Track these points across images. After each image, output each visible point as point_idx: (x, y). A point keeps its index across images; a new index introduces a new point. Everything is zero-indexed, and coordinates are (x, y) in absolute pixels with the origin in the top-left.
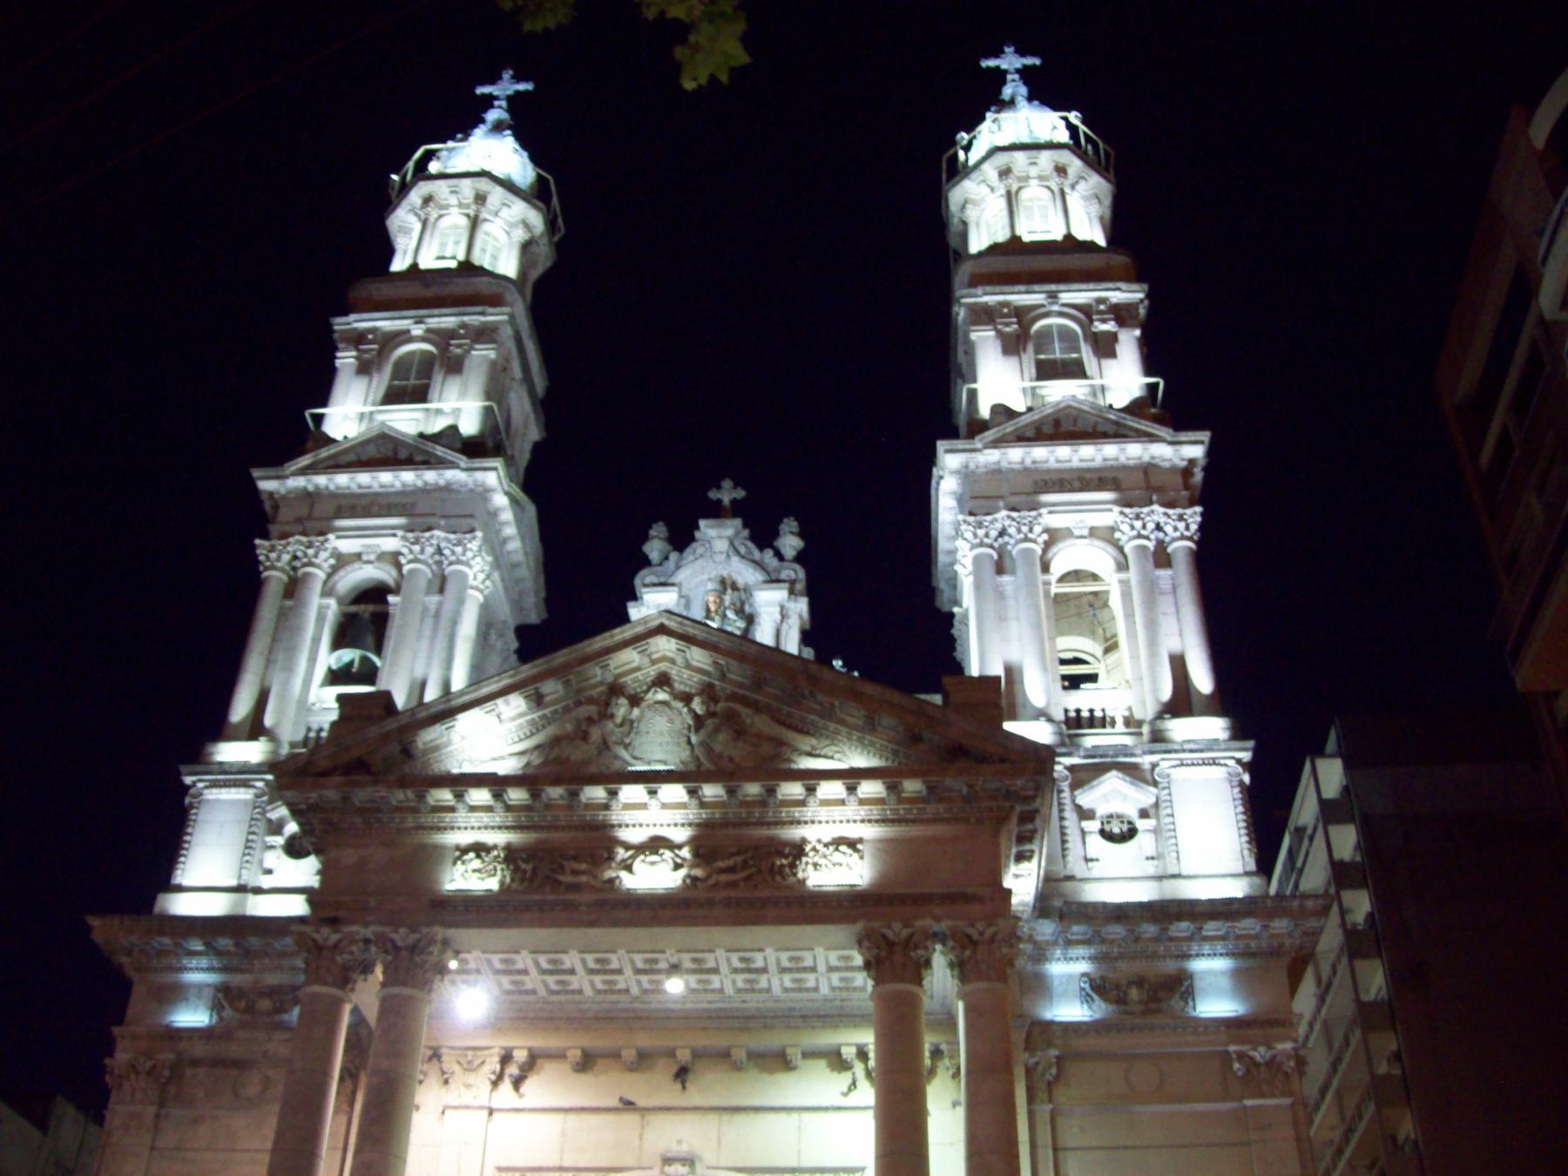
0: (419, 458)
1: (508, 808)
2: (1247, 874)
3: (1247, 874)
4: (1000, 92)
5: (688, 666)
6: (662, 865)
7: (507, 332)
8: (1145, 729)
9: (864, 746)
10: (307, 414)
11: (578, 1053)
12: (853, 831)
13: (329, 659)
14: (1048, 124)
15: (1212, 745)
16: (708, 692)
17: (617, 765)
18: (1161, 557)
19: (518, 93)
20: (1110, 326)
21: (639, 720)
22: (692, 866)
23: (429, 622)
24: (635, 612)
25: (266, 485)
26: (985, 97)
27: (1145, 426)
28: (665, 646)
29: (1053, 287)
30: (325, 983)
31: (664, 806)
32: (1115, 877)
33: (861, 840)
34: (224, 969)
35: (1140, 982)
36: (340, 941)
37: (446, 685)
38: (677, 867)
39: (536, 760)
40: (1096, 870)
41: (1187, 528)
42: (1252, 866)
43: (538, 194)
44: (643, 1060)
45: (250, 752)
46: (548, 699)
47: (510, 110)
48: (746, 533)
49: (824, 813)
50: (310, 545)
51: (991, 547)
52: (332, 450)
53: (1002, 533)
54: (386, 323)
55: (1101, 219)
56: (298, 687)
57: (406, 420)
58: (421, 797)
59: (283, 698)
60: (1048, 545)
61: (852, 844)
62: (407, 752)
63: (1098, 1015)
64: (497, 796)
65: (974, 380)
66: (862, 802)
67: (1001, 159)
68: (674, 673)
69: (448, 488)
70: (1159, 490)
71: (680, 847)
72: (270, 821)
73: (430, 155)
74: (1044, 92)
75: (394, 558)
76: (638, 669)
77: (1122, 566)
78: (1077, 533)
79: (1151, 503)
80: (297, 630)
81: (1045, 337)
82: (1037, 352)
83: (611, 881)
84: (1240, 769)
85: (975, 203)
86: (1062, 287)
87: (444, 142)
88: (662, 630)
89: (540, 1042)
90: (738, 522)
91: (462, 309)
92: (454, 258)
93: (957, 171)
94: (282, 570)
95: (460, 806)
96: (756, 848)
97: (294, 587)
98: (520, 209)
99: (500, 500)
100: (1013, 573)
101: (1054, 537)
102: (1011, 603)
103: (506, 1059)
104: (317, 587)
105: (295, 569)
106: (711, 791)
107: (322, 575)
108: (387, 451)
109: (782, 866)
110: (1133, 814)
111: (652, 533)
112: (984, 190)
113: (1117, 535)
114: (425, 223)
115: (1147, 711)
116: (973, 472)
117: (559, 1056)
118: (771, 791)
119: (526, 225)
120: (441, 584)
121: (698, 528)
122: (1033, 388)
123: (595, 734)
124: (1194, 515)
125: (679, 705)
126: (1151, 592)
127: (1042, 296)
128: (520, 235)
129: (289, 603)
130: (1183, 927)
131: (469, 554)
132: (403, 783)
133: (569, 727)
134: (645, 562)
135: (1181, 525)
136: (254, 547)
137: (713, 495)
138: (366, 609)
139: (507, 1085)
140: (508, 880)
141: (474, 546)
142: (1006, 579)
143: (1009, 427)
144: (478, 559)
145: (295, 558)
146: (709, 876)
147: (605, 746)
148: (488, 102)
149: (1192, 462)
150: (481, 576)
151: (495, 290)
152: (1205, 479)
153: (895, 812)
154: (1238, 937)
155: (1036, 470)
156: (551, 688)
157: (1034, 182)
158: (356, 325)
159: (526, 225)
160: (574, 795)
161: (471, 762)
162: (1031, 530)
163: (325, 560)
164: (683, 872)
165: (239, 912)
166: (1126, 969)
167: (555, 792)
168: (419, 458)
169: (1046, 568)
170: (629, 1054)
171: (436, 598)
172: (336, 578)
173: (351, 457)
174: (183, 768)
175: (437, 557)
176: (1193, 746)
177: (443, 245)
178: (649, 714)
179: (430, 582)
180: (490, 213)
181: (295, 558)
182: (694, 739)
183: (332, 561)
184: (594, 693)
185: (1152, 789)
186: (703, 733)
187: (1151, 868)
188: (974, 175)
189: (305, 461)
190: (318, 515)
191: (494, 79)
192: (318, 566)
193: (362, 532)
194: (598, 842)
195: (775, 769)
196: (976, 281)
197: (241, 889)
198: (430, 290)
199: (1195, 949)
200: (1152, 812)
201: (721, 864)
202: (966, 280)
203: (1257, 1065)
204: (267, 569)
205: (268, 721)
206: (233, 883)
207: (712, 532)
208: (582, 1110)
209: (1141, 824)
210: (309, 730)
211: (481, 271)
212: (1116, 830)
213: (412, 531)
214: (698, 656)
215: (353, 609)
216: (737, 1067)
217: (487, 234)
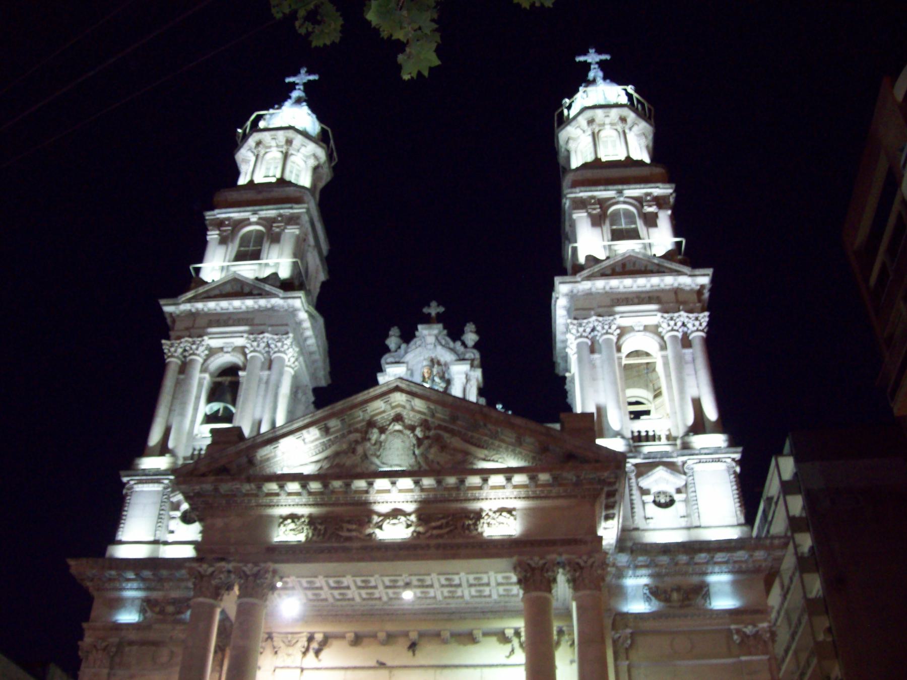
0: (255, 292)
2: (739, 525)
3: (739, 525)
4: (587, 75)
5: (413, 409)
6: (400, 525)
7: (305, 218)
8: (679, 442)
9: (515, 454)
10: (191, 267)
11: (352, 635)
12: (510, 504)
13: (205, 409)
14: (616, 93)
15: (717, 450)
16: (425, 425)
17: (373, 468)
18: (686, 342)
19: (309, 81)
20: (653, 209)
21: (385, 441)
23: (263, 386)
25: (168, 309)
26: (579, 78)
27: (675, 266)
29: (620, 187)
30: (205, 596)
32: (662, 528)
33: (514, 509)
34: (147, 589)
35: (678, 589)
36: (213, 572)
37: (273, 423)
38: (408, 526)
39: (326, 465)
40: (651, 524)
41: (701, 324)
42: (742, 520)
43: (322, 139)
44: (390, 639)
45: (161, 463)
46: (332, 430)
47: (305, 91)
48: (445, 332)
49: (493, 494)
50: (194, 343)
51: (587, 337)
52: (206, 288)
53: (593, 330)
54: (235, 214)
55: (647, 147)
56: (188, 425)
57: (248, 270)
58: (260, 488)
60: (620, 336)
61: (510, 511)
62: (251, 462)
64: (304, 486)
65: (576, 242)
66: (515, 487)
67: (589, 114)
68: (405, 413)
69: (273, 309)
70: (684, 303)
71: (410, 514)
72: (172, 503)
73: (260, 118)
74: (613, 74)
75: (242, 350)
76: (384, 412)
77: (663, 347)
78: (636, 328)
79: (679, 311)
80: (186, 392)
81: (616, 216)
82: (612, 225)
83: (370, 535)
84: (734, 464)
85: (574, 139)
86: (625, 187)
87: (268, 109)
88: (397, 389)
89: (330, 629)
90: (440, 326)
91: (279, 206)
92: (274, 176)
93: (563, 122)
94: (177, 357)
95: (282, 493)
96: (454, 515)
97: (185, 367)
98: (312, 148)
99: (303, 315)
100: (600, 352)
102: (599, 370)
103: (311, 639)
104: (198, 367)
105: (185, 357)
106: (427, 482)
107: (200, 360)
109: (469, 525)
110: (671, 490)
111: (391, 333)
112: (579, 131)
113: (660, 330)
114: (257, 157)
115: (679, 432)
116: (576, 295)
117: (341, 637)
118: (462, 481)
120: (269, 364)
121: (417, 329)
122: (610, 246)
123: (360, 450)
124: (704, 317)
125: (408, 432)
126: (680, 362)
127: (614, 192)
128: (312, 163)
129: (182, 377)
130: (702, 557)
131: (286, 347)
132: (249, 480)
133: (345, 446)
134: (387, 350)
135: (697, 323)
136: (161, 345)
137: (426, 310)
138: (227, 379)
139: (311, 654)
140: (310, 535)
141: (288, 342)
142: (596, 356)
143: (597, 268)
144: (291, 350)
145: (185, 350)
146: (426, 532)
147: (365, 457)
148: (293, 86)
149: (702, 287)
150: (293, 360)
151: (298, 194)
152: (710, 296)
153: (535, 492)
154: (735, 562)
155: (612, 293)
156: (334, 423)
157: (607, 127)
159: (315, 157)
160: (348, 485)
161: (288, 467)
162: (610, 328)
163: (202, 351)
164: (412, 529)
165: (154, 555)
166: (669, 581)
167: (337, 484)
168: (255, 292)
169: (619, 349)
170: (382, 635)
171: (266, 373)
172: (209, 362)
173: (217, 292)
174: (122, 473)
175: (267, 349)
176: (706, 451)
177: (268, 169)
178: (390, 438)
179: (263, 363)
181: (185, 350)
182: (417, 452)
183: (207, 352)
184: (359, 426)
185: (684, 477)
186: (422, 448)
187: (683, 522)
188: (574, 123)
189: (190, 295)
190: (198, 326)
192: (199, 355)
193: (223, 335)
194: (362, 513)
195: (464, 469)
196: (576, 184)
197: (156, 542)
198: (260, 195)
199: (710, 569)
200: (683, 490)
201: (433, 524)
202: (569, 184)
203: (748, 637)
204: (169, 357)
205: (171, 445)
206: (151, 539)
207: (425, 332)
208: (355, 668)
209: (677, 497)
210: (194, 449)
211: (290, 184)
212: (663, 501)
213: (252, 334)
214: (419, 404)
215: (219, 379)
216: (445, 642)
217: (294, 163)
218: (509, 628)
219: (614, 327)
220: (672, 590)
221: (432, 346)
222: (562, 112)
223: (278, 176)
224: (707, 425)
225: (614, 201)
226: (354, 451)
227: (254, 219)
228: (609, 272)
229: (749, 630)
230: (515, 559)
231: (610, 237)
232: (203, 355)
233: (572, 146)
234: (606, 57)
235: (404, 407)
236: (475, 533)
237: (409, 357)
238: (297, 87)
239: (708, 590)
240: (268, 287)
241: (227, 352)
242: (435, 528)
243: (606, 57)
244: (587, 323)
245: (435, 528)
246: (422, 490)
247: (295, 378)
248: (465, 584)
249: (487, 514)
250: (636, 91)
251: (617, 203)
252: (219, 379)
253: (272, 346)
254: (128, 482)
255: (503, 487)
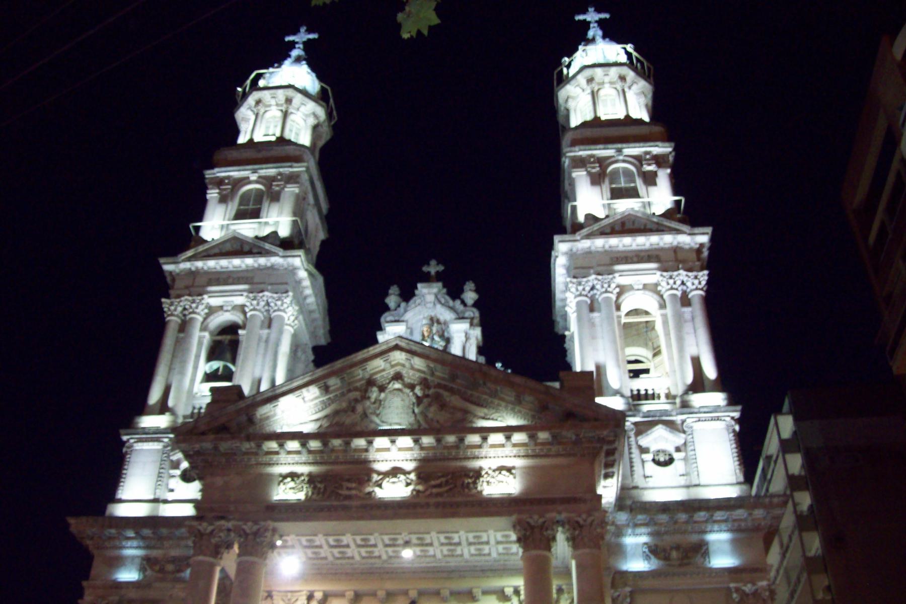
0: (255, 250)
1: (310, 452)
2: (738, 483)
4: (586, 34)
5: (412, 368)
6: (399, 484)
7: (305, 177)
8: (678, 401)
10: (191, 226)
11: (352, 593)
12: (509, 463)
13: (205, 367)
14: (615, 52)
15: (716, 409)
16: (424, 383)
17: (372, 426)
18: (685, 300)
19: (309, 40)
20: (652, 168)
21: (385, 399)
22: (417, 484)
23: (263, 345)
24: (381, 337)
25: (168, 268)
26: (578, 37)
27: (674, 225)
28: (399, 357)
29: (619, 146)
30: (205, 555)
31: (400, 449)
32: (662, 486)
33: (514, 468)
35: (677, 548)
36: (213, 531)
37: (273, 381)
38: (408, 484)
39: (326, 424)
40: (651, 483)
41: (700, 283)
42: (741, 479)
43: (322, 98)
45: (161, 421)
46: (331, 389)
47: (305, 50)
48: (445, 290)
49: (492, 452)
50: (194, 302)
51: (586, 296)
52: (206, 246)
53: (593, 288)
54: (235, 173)
55: (647, 106)
56: (188, 383)
57: (248, 229)
58: (259, 446)
59: (179, 389)
60: (619, 295)
61: (509, 470)
62: (251, 421)
63: (653, 567)
64: (303, 445)
65: (575, 200)
66: (515, 445)
67: (588, 73)
68: (404, 372)
69: (272, 268)
70: (683, 261)
71: (409, 473)
72: (172, 461)
73: (259, 76)
74: (612, 33)
75: (242, 308)
76: (383, 370)
77: (663, 306)
79: (678, 269)
81: (616, 172)
82: (611, 183)
83: (370, 493)
84: (733, 423)
85: (573, 98)
86: (624, 145)
87: (267, 68)
88: (397, 347)
90: (440, 284)
92: (274, 135)
93: (562, 80)
94: (177, 316)
97: (184, 326)
99: (303, 274)
100: (599, 311)
101: (623, 290)
102: (599, 329)
105: (185, 315)
106: (427, 440)
107: (200, 319)
108: (237, 247)
109: (468, 483)
110: (671, 449)
111: (390, 291)
113: (659, 288)
114: (257, 115)
115: (679, 390)
116: (575, 254)
118: (462, 440)
119: (315, 116)
120: (269, 323)
121: (416, 288)
122: (609, 204)
123: (359, 408)
124: (704, 276)
125: (407, 391)
126: (680, 321)
128: (312, 121)
129: (182, 335)
130: (701, 515)
131: (285, 306)
132: (248, 438)
133: (344, 405)
134: (387, 308)
135: (696, 282)
136: (161, 303)
137: (425, 269)
138: (227, 338)
140: (310, 494)
141: (288, 301)
143: (596, 227)
144: (290, 308)
145: (185, 309)
146: (426, 490)
147: (365, 415)
148: (292, 45)
149: (702, 245)
150: (292, 318)
151: (298, 153)
153: (534, 451)
154: (735, 520)
156: (333, 382)
157: (607, 86)
158: (218, 175)
159: (315, 116)
160: (348, 444)
161: (288, 425)
162: (609, 286)
163: (202, 310)
164: (411, 487)
166: (669, 540)
167: (337, 443)
168: (255, 250)
169: (618, 308)
171: (266, 331)
172: (209, 320)
173: (216, 251)
174: (122, 431)
175: (267, 308)
177: (268, 128)
178: (390, 396)
179: (263, 322)
180: (294, 108)
181: (185, 309)
182: (416, 410)
183: (206, 311)
184: (358, 384)
185: (683, 435)
186: (422, 406)
187: (682, 481)
188: (573, 82)
189: (190, 253)
190: (198, 284)
191: (295, 32)
192: (198, 314)
193: (223, 294)
194: (362, 471)
195: (463, 427)
196: (575, 143)
197: (156, 501)
198: (260, 153)
200: (683, 448)
201: (433, 483)
202: (569, 142)
203: (747, 595)
204: (169, 315)
205: (171, 403)
206: (151, 497)
207: (425, 291)
209: (676, 456)
210: (194, 408)
211: (289, 142)
212: (662, 459)
214: (418, 363)
215: (219, 338)
217: (293, 121)
218: (508, 586)
219: (613, 286)
220: (672, 548)
221: (431, 305)
222: (561, 71)
223: (278, 134)
224: (706, 383)
225: (613, 159)
226: (353, 410)
227: (254, 177)
228: (608, 230)
229: (748, 588)
230: (514, 518)
231: (609, 195)
232: (203, 313)
233: (571, 104)
234: (606, 16)
235: (403, 366)
236: (474, 491)
237: (408, 316)
238: (297, 46)
239: (707, 549)
240: (267, 246)
241: (227, 311)
242: (434, 486)
243: (606, 16)
244: (587, 282)
245: (434, 486)
246: (422, 448)
247: (295, 336)
248: (464, 543)
249: (487, 473)
250: (635, 50)
251: (616, 162)
252: (219, 338)
253: (272, 304)
254: (128, 440)
255: (503, 446)
